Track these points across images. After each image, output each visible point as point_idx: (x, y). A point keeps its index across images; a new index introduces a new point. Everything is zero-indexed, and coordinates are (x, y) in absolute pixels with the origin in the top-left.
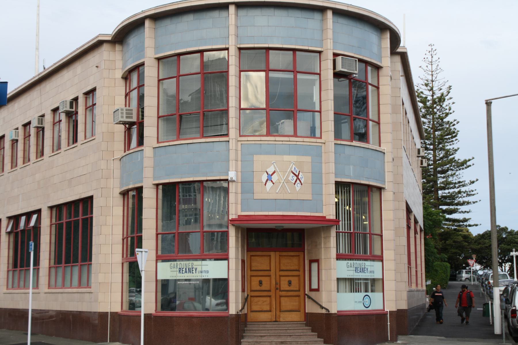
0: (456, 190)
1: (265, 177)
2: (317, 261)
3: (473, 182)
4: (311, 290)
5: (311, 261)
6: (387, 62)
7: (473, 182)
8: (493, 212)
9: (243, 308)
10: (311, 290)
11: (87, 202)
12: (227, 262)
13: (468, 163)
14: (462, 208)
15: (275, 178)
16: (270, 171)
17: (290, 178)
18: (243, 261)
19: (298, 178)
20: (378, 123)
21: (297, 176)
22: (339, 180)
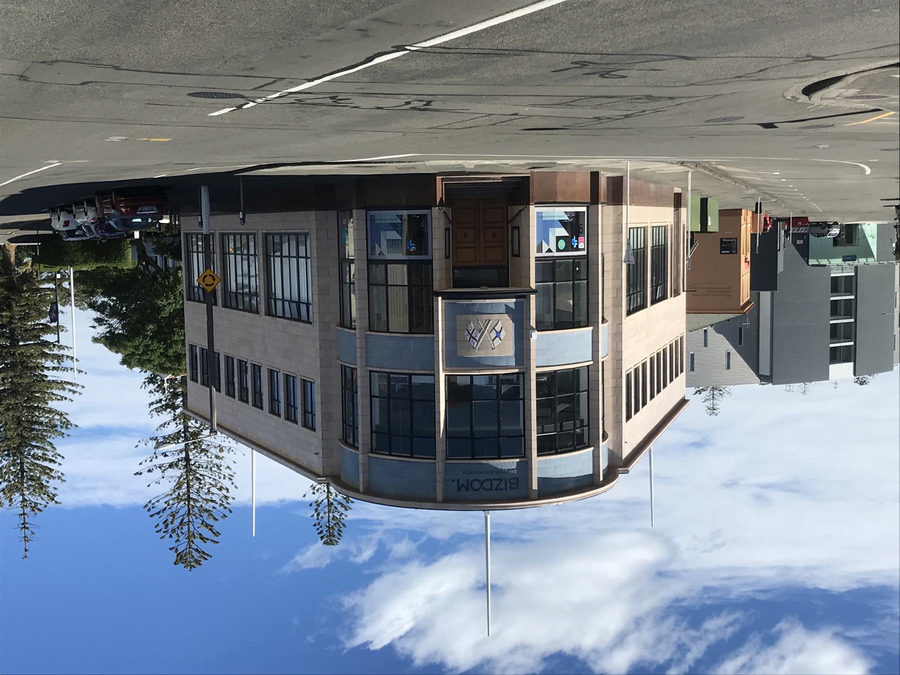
1: (502, 335)
15: (493, 334)
16: (498, 328)
20: (371, 396)
21: (471, 337)
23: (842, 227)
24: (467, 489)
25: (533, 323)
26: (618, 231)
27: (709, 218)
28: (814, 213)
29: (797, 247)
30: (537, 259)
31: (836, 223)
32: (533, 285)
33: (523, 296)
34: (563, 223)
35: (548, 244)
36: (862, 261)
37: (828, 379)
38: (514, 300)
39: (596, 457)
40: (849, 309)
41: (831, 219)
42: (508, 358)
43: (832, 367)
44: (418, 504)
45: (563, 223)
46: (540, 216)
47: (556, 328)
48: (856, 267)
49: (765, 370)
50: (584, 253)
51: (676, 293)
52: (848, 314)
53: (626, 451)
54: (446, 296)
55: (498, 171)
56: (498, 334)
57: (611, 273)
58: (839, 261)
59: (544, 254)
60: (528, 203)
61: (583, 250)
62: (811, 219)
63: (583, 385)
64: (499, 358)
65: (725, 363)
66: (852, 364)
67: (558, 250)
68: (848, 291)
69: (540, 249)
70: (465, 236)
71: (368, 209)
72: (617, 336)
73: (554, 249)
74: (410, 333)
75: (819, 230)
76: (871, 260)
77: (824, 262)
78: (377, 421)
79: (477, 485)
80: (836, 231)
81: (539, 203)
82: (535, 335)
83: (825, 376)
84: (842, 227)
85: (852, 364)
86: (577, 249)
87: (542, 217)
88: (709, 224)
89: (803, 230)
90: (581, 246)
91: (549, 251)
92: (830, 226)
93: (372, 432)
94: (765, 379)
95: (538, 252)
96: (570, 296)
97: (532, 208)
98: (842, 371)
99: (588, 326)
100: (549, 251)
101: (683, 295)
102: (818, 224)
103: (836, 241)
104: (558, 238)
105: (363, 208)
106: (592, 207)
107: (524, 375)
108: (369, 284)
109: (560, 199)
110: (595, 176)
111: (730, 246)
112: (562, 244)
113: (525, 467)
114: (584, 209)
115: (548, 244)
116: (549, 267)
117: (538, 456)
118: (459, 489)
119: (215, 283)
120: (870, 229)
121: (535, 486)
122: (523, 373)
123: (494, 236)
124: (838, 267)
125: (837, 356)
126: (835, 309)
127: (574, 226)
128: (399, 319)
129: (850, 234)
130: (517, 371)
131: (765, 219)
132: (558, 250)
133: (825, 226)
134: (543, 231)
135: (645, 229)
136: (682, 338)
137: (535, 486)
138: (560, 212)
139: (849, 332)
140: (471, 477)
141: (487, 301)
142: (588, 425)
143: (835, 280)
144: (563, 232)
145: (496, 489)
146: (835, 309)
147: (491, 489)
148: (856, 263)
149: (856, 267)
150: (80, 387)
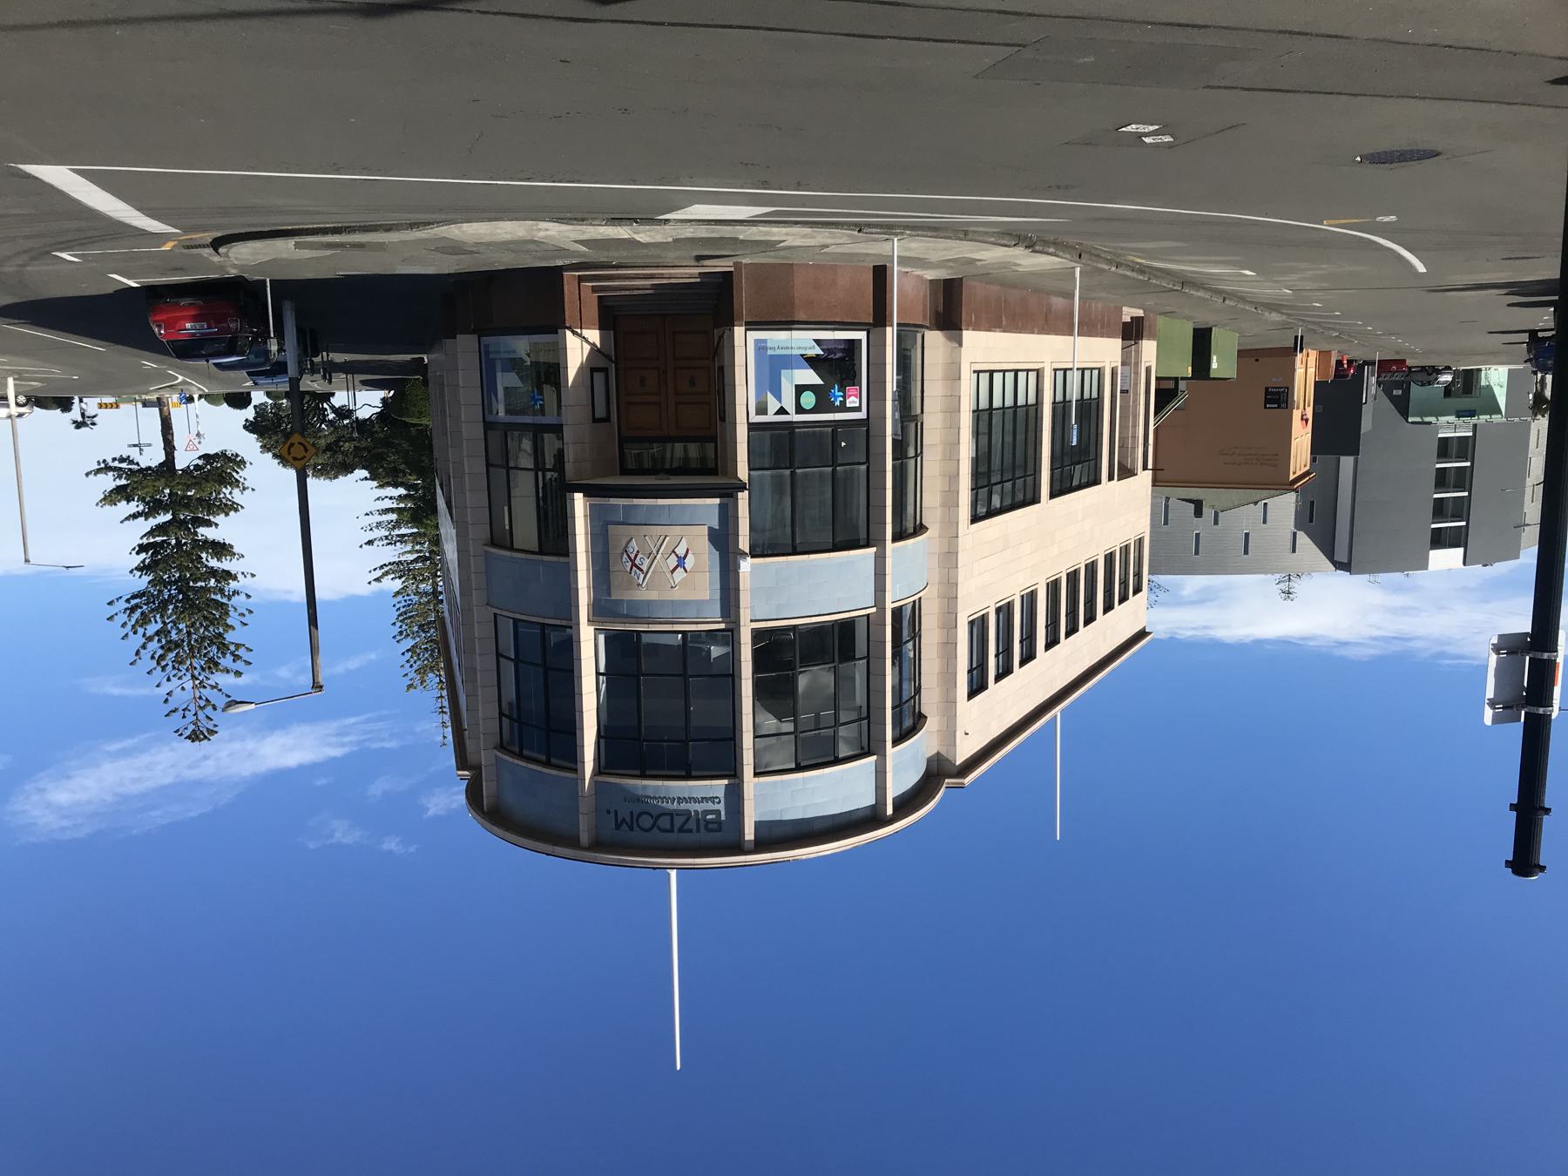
0: (397, 532)
1: (689, 562)
2: (595, 420)
3: (370, 543)
4: (605, 370)
5: (607, 419)
6: (486, 756)
7: (370, 543)
8: (1059, 417)
9: (721, 337)
10: (605, 370)
11: (975, 519)
12: (534, 546)
13: (379, 573)
14: (388, 504)
15: (673, 561)
16: (681, 551)
17: (647, 562)
18: (723, 419)
19: (633, 561)
20: (499, 655)
21: (634, 565)
22: (563, 559)
23: (1456, 374)
24: (631, 829)
25: (744, 544)
26: (954, 376)
27: (1214, 358)
28: (1413, 354)
29: (1393, 399)
30: (752, 427)
31: (1449, 368)
32: (743, 472)
33: (728, 492)
34: (812, 362)
35: (779, 399)
36: (1484, 418)
37: (1425, 567)
38: (717, 501)
39: (880, 773)
40: (1462, 479)
41: (1439, 362)
42: (700, 603)
43: (1432, 553)
44: (549, 848)
45: (812, 362)
46: (761, 347)
47: (795, 553)
48: (1475, 426)
49: (1341, 556)
50: (862, 415)
51: (1126, 472)
52: (1459, 486)
53: (962, 754)
54: (589, 491)
55: (640, 261)
56: (681, 562)
57: (940, 448)
58: (1452, 419)
59: (770, 417)
60: (731, 324)
61: (858, 409)
62: (1409, 362)
63: (861, 647)
64: (685, 603)
65: (1289, 545)
66: (1461, 550)
67: (800, 410)
68: (1462, 456)
69: (762, 410)
70: (692, 382)
71: (481, 332)
72: (949, 557)
73: (791, 407)
74: (541, 552)
75: (1424, 377)
76: (1496, 418)
77: (1433, 419)
78: (510, 693)
79: (646, 822)
80: (1447, 378)
81: (752, 325)
82: (746, 565)
83: (1423, 564)
84: (1456, 374)
85: (1461, 550)
86: (843, 408)
87: (765, 348)
88: (1214, 365)
89: (1398, 377)
90: (852, 402)
91: (782, 411)
92: (1439, 372)
93: (501, 714)
94: (1345, 566)
95: (758, 413)
96: (834, 487)
97: (739, 331)
98: (1446, 559)
99: (867, 546)
100: (782, 411)
101: (1144, 478)
102: (1423, 368)
103: (1448, 391)
104: (800, 389)
105: (473, 332)
106: (874, 331)
107: (730, 635)
108: (488, 465)
109: (801, 316)
110: (880, 274)
111: (1279, 398)
112: (809, 400)
113: (735, 796)
114: (861, 335)
115: (779, 399)
116: (778, 443)
117: (756, 774)
118: (618, 827)
119: (308, 455)
120: (1496, 377)
121: (749, 834)
122: (732, 630)
123: (692, 382)
124: (1451, 427)
125: (1440, 540)
126: (1442, 479)
127: (837, 366)
128: (526, 530)
129: (1468, 381)
130: (722, 626)
131: (1339, 363)
132: (800, 410)
133: (1429, 373)
134: (767, 374)
135: (1039, 373)
136: (1140, 541)
137: (749, 834)
138: (804, 341)
139: (1460, 509)
140: (637, 809)
141: (661, 502)
142: (868, 717)
143: (1444, 442)
144: (810, 377)
145: (681, 830)
146: (1442, 479)
147: (672, 830)
148: (1474, 420)
149: (1475, 426)
150: (243, 597)
